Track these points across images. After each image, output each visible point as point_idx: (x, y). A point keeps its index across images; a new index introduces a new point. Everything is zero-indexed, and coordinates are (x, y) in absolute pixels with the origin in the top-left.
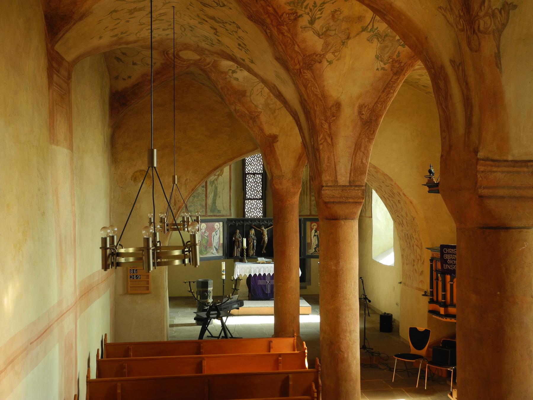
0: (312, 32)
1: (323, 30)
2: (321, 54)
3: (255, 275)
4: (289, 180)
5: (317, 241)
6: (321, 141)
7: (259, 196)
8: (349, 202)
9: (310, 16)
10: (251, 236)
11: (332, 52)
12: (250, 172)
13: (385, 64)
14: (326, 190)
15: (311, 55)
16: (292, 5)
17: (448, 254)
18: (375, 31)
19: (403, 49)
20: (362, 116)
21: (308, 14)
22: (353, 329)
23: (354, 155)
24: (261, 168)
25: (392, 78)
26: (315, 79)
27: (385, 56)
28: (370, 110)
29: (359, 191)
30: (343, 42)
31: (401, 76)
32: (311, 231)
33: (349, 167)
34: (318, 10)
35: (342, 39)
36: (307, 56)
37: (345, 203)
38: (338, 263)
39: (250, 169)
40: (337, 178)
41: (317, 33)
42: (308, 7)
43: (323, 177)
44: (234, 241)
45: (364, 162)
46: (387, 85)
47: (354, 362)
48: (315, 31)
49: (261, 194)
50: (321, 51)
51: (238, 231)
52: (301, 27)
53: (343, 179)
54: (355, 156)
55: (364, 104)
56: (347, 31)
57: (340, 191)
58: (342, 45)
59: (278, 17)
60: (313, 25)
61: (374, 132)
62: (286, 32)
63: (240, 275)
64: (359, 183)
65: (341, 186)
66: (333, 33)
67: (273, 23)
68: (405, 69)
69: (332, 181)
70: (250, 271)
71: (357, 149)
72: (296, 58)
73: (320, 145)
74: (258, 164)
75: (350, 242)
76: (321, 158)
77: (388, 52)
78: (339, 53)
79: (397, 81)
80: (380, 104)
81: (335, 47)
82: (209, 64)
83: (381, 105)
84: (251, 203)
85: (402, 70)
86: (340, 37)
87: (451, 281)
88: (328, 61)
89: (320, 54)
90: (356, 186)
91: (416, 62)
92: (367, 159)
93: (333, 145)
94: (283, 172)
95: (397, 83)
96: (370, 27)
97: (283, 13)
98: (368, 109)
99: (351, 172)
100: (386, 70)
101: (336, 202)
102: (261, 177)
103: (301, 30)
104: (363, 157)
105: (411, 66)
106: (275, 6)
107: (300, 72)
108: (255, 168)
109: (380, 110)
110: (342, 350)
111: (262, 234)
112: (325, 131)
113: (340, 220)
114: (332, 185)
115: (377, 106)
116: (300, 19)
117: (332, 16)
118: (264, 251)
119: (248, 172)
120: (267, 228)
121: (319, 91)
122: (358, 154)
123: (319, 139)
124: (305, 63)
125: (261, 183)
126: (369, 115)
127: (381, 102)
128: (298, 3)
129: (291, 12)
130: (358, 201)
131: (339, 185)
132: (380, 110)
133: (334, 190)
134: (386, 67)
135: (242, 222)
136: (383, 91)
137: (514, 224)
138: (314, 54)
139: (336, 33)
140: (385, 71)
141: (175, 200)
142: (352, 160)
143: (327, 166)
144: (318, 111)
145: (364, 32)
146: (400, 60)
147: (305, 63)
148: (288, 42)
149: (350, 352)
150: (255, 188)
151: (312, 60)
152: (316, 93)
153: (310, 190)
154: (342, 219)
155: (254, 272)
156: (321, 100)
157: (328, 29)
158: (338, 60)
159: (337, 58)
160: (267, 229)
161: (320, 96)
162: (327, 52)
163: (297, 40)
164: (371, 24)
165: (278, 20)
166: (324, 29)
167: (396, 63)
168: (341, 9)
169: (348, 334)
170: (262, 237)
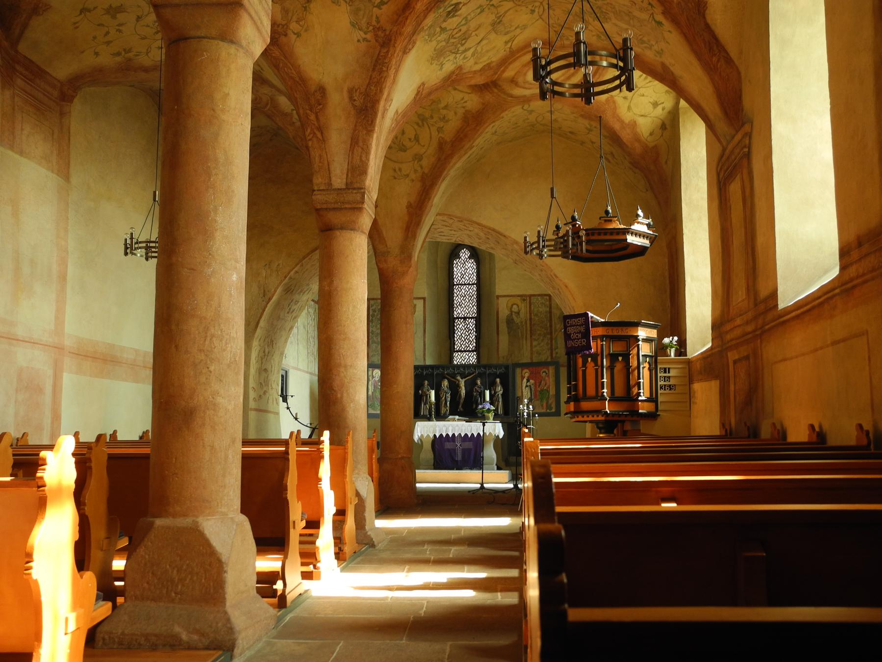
3: (441, 435)
4: (396, 257)
5: (529, 394)
6: (309, 135)
7: (471, 347)
8: (346, 208)
10: (443, 389)
12: (460, 316)
13: (365, 33)
14: (318, 194)
17: (571, 326)
19: (380, 11)
20: (354, 103)
22: (350, 364)
24: (474, 310)
25: (380, 52)
26: (285, 57)
29: (358, 195)
30: (304, 7)
31: (391, 49)
32: (522, 380)
33: (346, 167)
37: (341, 209)
38: (331, 282)
39: (460, 312)
40: (331, 180)
44: (421, 396)
45: (363, 160)
47: (352, 405)
49: (474, 344)
50: (282, 19)
51: (426, 382)
53: (338, 182)
54: (353, 153)
58: (305, 11)
61: (372, 122)
63: (422, 435)
64: (358, 185)
65: (336, 189)
69: (325, 184)
70: (435, 430)
71: (353, 144)
74: (470, 305)
75: (347, 256)
76: (311, 157)
80: (373, 86)
81: (298, 15)
82: (267, 104)
84: (461, 356)
85: (390, 40)
87: (583, 367)
88: (295, 34)
89: (281, 24)
90: (354, 189)
91: (403, 28)
92: (367, 156)
93: (324, 140)
94: (389, 247)
98: (361, 93)
99: (348, 172)
100: (370, 41)
101: (330, 209)
102: (474, 322)
104: (361, 153)
108: (467, 310)
110: (334, 389)
111: (458, 386)
115: (371, 89)
118: (460, 408)
119: (457, 316)
120: (465, 378)
122: (355, 150)
123: (307, 133)
125: (475, 330)
131: (333, 188)
133: (328, 194)
134: (368, 36)
135: (431, 370)
136: (374, 70)
137: (193, 33)
140: (369, 43)
141: (264, 290)
142: (349, 157)
143: (319, 166)
146: (382, 27)
149: (345, 392)
150: (466, 336)
153: (531, 333)
154: (337, 229)
155: (439, 431)
156: (300, 85)
158: (306, 30)
159: (304, 29)
160: (464, 380)
161: (297, 79)
167: (379, 31)
169: (342, 369)
170: (458, 390)
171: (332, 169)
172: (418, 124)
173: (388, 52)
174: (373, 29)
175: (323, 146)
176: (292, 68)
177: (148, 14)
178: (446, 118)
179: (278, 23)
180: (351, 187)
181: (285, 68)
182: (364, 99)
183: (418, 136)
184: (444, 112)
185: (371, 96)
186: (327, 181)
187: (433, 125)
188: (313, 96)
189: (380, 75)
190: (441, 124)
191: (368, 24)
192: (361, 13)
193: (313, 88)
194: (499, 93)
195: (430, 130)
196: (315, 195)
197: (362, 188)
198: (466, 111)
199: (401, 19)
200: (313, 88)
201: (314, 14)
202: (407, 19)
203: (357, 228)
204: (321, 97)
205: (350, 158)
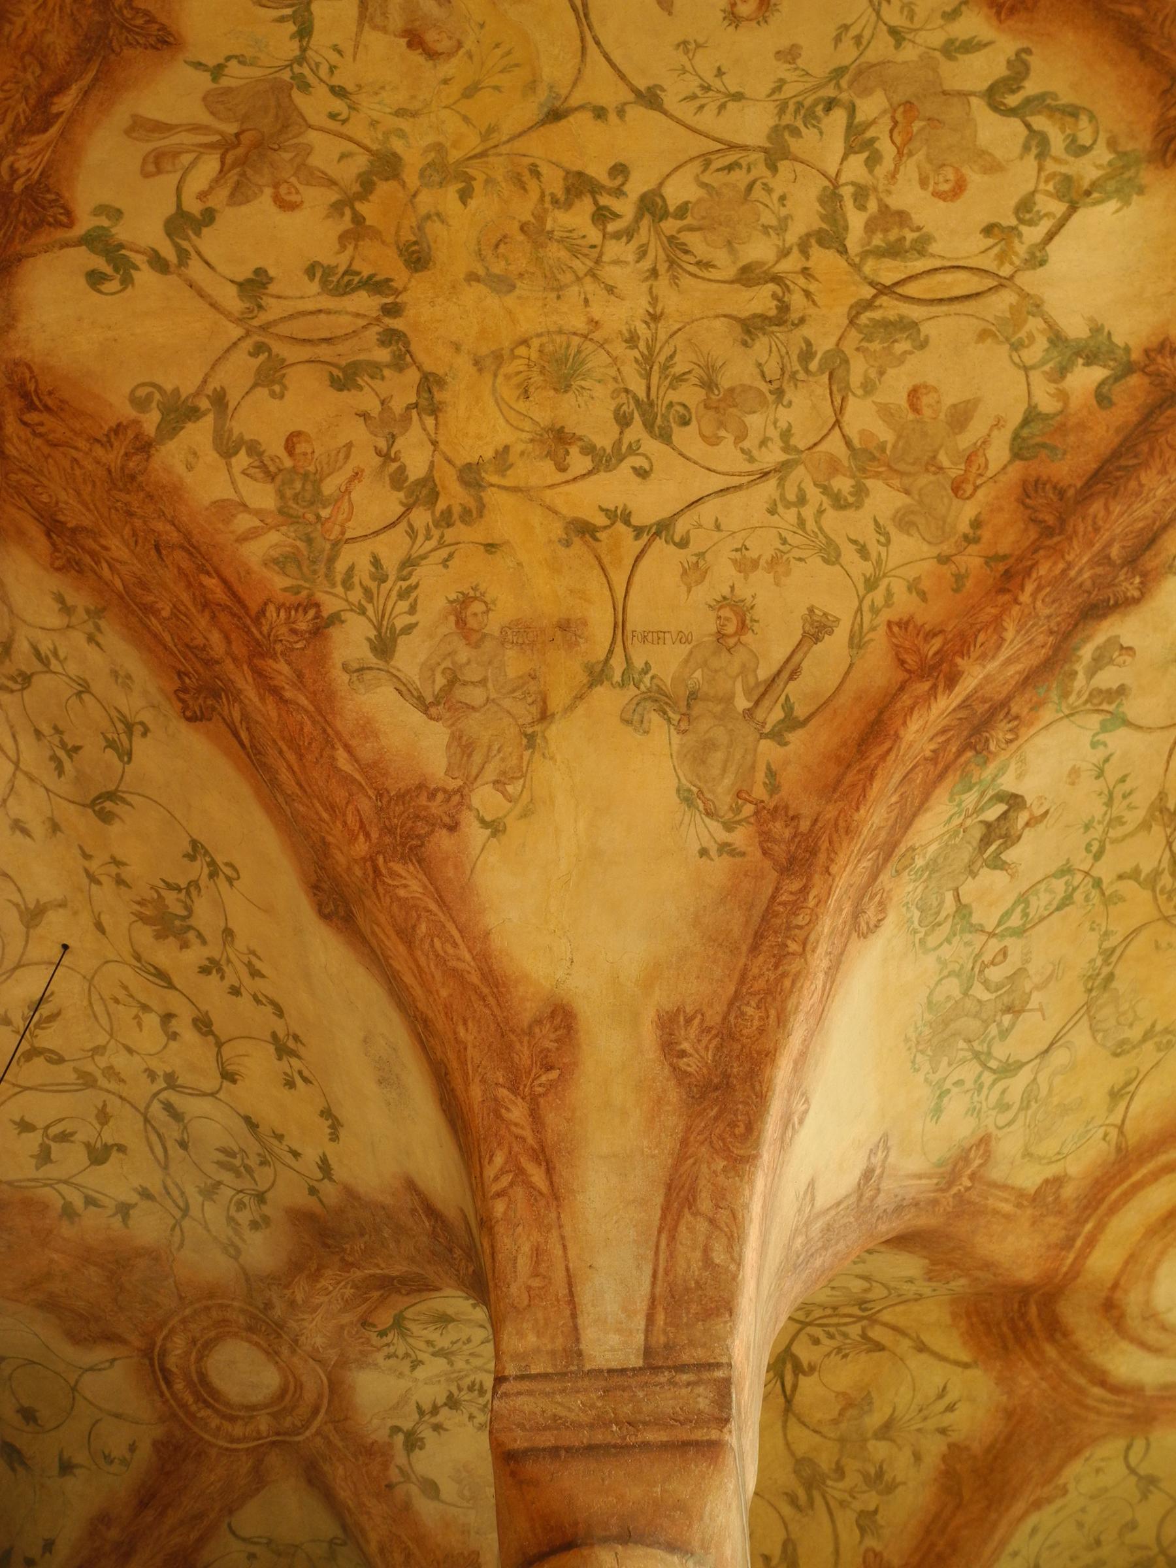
0: (392, 689)
1: (434, 682)
2: (450, 788)
6: (496, 1178)
8: (646, 1446)
9: (370, 621)
11: (494, 778)
13: (729, 827)
14: (519, 1393)
15: (408, 791)
16: (292, 569)
18: (641, 681)
19: (781, 751)
20: (682, 1063)
21: (363, 612)
23: (664, 1236)
25: (777, 889)
26: (442, 902)
27: (720, 790)
28: (714, 1032)
29: (700, 1390)
34: (394, 593)
35: (521, 721)
36: (391, 799)
37: (623, 1449)
40: (578, 1340)
41: (415, 693)
42: (356, 580)
43: (505, 1337)
45: (717, 1261)
46: (763, 919)
48: (405, 685)
50: (446, 773)
52: (345, 668)
54: (672, 1238)
55: (678, 1010)
56: (532, 687)
57: (594, 1396)
58: (527, 748)
59: (249, 622)
60: (391, 658)
61: (749, 1128)
62: (287, 687)
65: (601, 1371)
66: (476, 696)
67: (234, 647)
68: (824, 845)
69: (553, 1353)
72: (350, 807)
73: (493, 1198)
77: (724, 770)
78: (524, 786)
79: (805, 900)
80: (753, 1004)
82: (316, 1411)
83: (758, 1007)
85: (814, 852)
86: (509, 712)
88: (484, 823)
89: (445, 791)
90: (682, 1368)
91: (858, 809)
95: (809, 911)
96: (617, 664)
97: (266, 604)
100: (743, 854)
101: (568, 1450)
103: (345, 677)
104: (709, 1237)
105: (847, 833)
106: (228, 573)
107: (376, 870)
109: (761, 1031)
112: (517, 1137)
113: (592, 1545)
114: (550, 1370)
115: (743, 1014)
116: (335, 632)
117: (457, 623)
121: (468, 957)
122: (682, 1228)
123: (490, 1172)
124: (389, 831)
126: (714, 1055)
127: (758, 997)
128: (314, 562)
129: (292, 599)
130: (699, 1435)
131: (588, 1367)
132: (761, 1031)
133: (563, 1391)
136: (754, 949)
138: (421, 787)
139: (492, 697)
140: (738, 859)
143: (529, 1289)
144: (474, 1047)
145: (599, 689)
146: (786, 808)
147: (388, 830)
148: (305, 730)
151: (417, 817)
152: (453, 963)
154: (605, 1540)
157: (453, 681)
158: (525, 814)
159: (518, 810)
161: (475, 978)
162: (471, 781)
163: (339, 725)
164: (619, 649)
165: (248, 632)
166: (440, 681)
167: (774, 819)
168: (482, 587)
171: (585, 1296)
172: (793, 1500)
173: (805, 890)
174: (756, 813)
175: (553, 1215)
176: (459, 940)
177: (19, 966)
178: (886, 1477)
179: (433, 786)
180: (670, 1363)
181: (436, 940)
182: (718, 1049)
183: (795, 1550)
184: (880, 1450)
185: (745, 1040)
186: (560, 1342)
187: (843, 1504)
188: (526, 1039)
189: (776, 966)
190: (870, 1500)
191: (738, 795)
192: (719, 756)
193: (528, 1011)
194: (1064, 1366)
195: (833, 1521)
196: (505, 1395)
197: (718, 1365)
198: (951, 1446)
199: (849, 779)
200: (528, 1011)
201: (558, 757)
202: (871, 777)
203: (696, 1544)
204: (556, 1041)
205: (662, 1257)
